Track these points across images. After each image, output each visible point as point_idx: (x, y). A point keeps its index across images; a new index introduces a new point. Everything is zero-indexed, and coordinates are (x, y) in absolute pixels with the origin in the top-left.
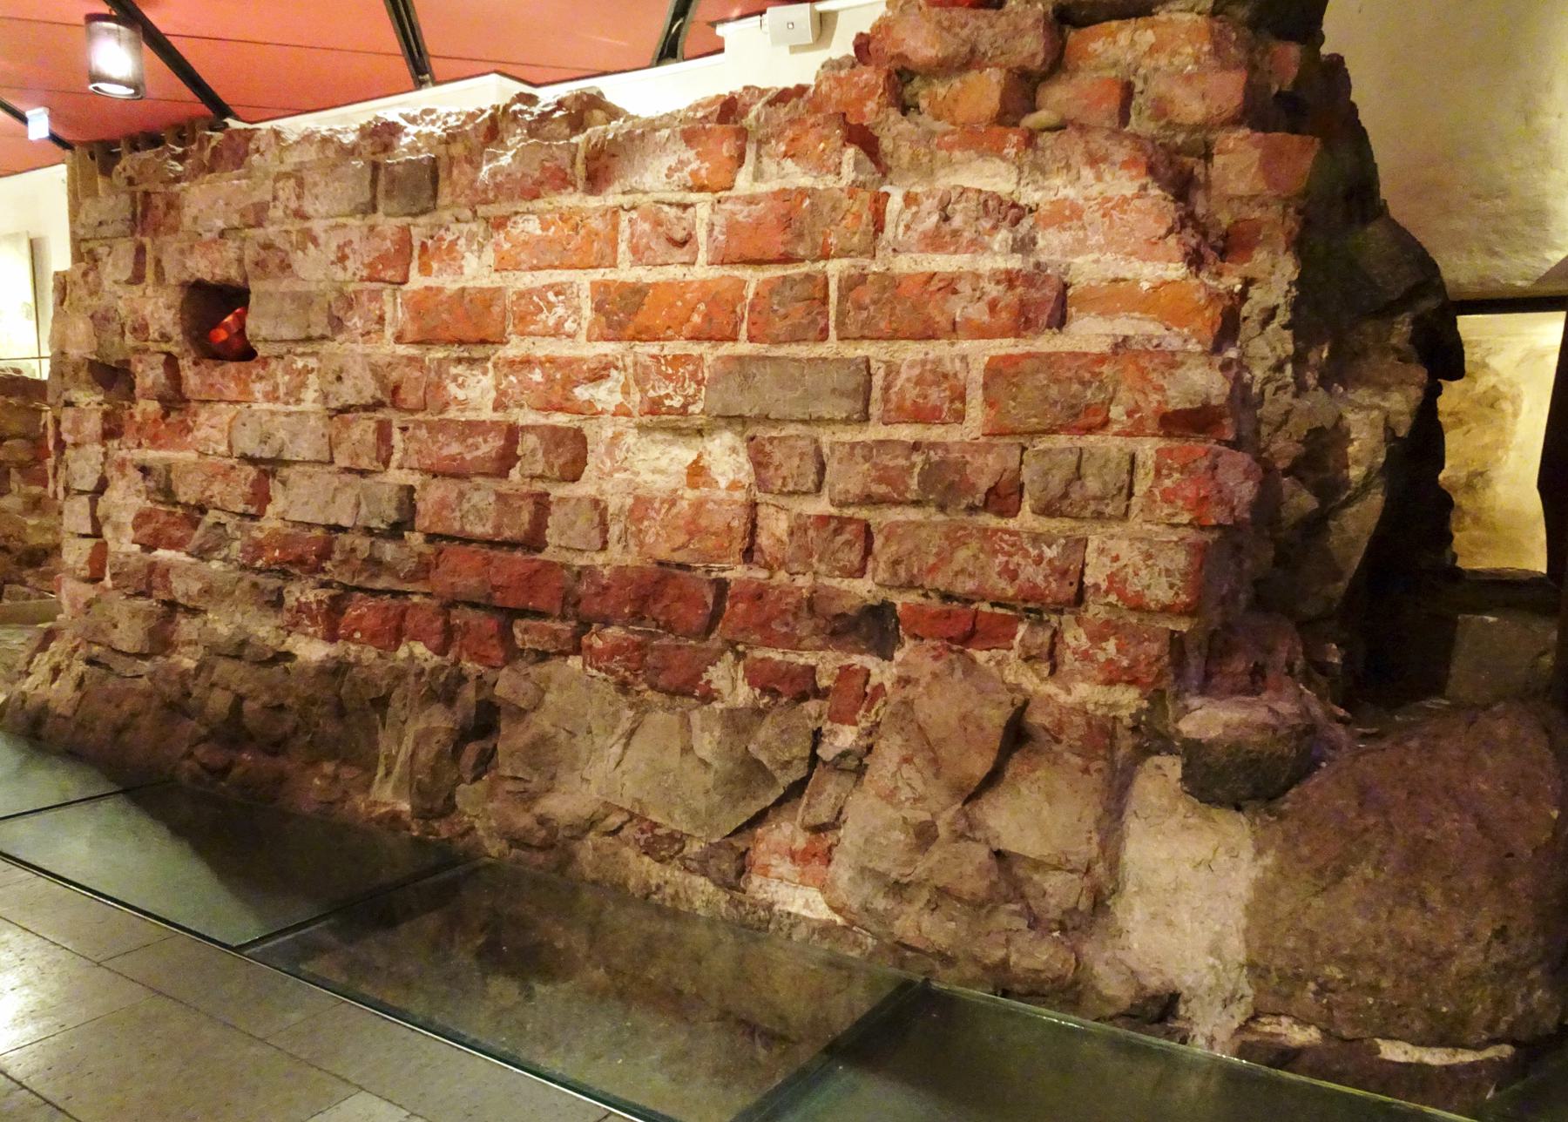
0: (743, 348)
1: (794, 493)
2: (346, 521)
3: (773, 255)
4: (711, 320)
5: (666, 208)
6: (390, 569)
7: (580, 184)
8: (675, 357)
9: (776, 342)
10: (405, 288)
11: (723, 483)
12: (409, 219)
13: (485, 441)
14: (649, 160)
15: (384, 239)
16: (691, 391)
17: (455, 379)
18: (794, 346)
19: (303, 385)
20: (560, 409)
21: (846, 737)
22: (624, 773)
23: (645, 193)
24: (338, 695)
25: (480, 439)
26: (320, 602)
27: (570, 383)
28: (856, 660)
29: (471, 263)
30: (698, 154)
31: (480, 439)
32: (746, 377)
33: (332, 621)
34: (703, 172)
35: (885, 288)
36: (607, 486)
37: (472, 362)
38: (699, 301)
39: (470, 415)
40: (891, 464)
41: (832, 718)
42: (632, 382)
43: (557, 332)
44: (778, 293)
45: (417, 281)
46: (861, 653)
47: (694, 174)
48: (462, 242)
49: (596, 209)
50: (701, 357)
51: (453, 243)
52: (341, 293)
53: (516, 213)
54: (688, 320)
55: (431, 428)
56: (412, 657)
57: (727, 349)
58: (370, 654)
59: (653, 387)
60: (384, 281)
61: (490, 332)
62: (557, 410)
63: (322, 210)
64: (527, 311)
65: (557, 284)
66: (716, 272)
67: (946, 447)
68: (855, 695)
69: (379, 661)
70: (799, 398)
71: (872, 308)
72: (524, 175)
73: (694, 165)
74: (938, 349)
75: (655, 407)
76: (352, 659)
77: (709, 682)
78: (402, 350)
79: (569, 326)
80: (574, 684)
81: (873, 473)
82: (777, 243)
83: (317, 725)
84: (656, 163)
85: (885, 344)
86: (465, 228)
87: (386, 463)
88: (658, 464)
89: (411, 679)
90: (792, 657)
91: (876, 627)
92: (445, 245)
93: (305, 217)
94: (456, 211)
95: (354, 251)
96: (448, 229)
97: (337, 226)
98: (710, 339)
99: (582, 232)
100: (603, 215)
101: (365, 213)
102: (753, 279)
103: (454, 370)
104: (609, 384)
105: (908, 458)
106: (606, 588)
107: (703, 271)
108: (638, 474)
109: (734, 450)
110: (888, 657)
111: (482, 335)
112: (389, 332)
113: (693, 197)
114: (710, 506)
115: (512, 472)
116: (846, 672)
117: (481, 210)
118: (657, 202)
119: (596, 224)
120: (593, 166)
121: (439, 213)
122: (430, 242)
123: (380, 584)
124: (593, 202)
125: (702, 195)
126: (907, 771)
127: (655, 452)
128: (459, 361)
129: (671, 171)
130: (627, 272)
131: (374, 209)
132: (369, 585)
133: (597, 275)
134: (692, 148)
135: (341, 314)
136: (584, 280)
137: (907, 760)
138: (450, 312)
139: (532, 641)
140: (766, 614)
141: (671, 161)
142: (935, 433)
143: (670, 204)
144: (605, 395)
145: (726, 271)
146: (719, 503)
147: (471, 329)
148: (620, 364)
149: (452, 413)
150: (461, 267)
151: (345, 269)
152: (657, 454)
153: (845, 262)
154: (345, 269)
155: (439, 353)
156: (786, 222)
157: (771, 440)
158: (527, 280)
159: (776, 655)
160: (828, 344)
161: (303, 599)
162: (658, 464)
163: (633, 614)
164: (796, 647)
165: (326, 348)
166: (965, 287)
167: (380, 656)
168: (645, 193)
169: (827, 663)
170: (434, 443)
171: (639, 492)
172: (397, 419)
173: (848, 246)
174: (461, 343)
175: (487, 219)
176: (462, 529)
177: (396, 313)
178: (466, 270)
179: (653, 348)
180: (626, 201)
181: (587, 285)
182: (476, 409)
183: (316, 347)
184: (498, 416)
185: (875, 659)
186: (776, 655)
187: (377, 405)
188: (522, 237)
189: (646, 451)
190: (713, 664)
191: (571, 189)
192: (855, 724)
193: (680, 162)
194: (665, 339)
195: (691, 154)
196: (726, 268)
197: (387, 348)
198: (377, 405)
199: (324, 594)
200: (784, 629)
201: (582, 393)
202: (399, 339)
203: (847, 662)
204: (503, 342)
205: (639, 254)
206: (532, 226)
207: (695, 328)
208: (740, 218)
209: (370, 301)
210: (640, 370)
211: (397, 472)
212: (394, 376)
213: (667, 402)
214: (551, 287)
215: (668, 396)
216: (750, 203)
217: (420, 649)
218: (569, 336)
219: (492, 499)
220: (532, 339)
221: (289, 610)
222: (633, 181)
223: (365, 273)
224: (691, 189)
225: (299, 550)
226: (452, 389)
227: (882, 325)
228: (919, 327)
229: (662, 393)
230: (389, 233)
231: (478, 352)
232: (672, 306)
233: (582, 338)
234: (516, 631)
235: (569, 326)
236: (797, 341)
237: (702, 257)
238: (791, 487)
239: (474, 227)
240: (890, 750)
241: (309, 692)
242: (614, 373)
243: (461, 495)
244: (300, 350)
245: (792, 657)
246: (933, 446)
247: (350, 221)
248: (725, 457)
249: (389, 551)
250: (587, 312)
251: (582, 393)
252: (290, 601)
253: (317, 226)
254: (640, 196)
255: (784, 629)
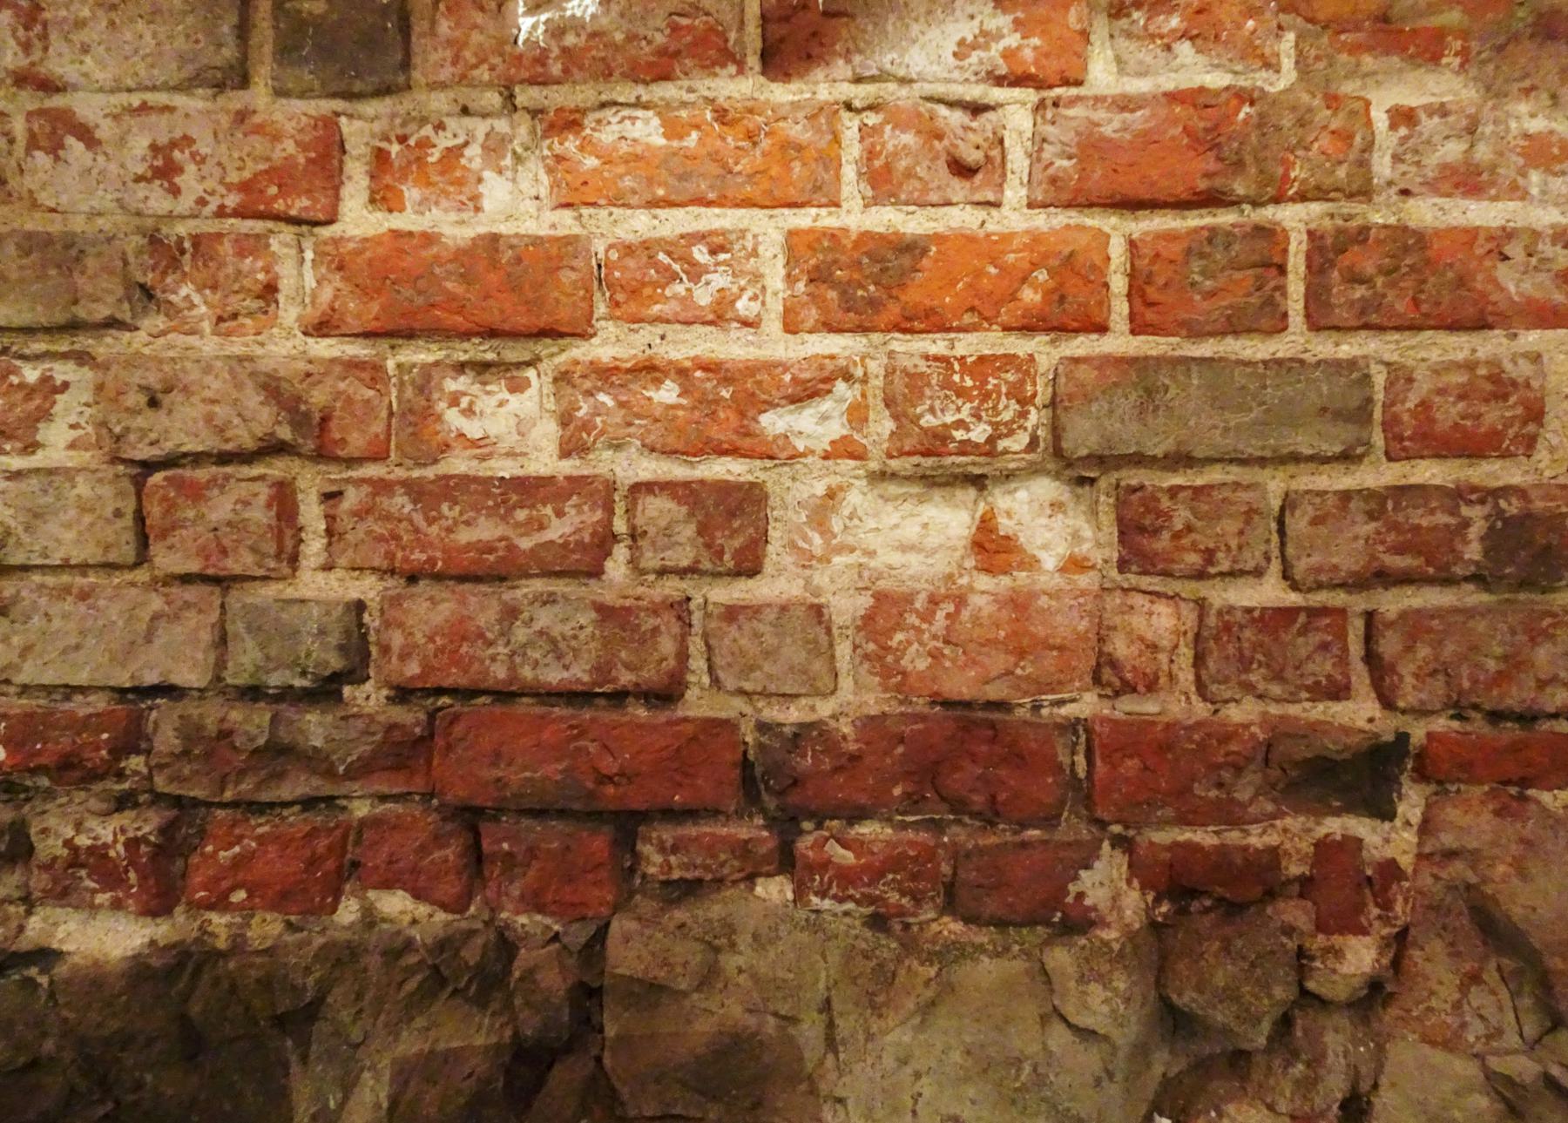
0: (1119, 342)
1: (1232, 574)
2: (189, 676)
3: (1181, 190)
4: (1062, 299)
5: (943, 111)
6: (316, 762)
7: (753, 61)
8: (982, 359)
9: (1195, 332)
10: (325, 232)
11: (1049, 562)
12: (338, 105)
13: (560, 514)
14: (915, 29)
15: (276, 138)
16: (1007, 416)
17: (454, 401)
18: (1230, 340)
19: (44, 415)
20: (734, 452)
21: (1361, 957)
22: (918, 1075)
23: (905, 81)
24: (184, 1019)
25: (548, 510)
26: (133, 844)
27: (751, 403)
28: (1333, 826)
29: (496, 192)
30: (1017, 22)
31: (548, 510)
32: (1149, 392)
33: (159, 878)
34: (1028, 54)
35: (1406, 249)
36: (821, 578)
37: (482, 368)
38: (1035, 266)
39: (505, 469)
40: (1424, 523)
41: (1321, 927)
42: (876, 403)
43: (720, 315)
44: (1202, 255)
45: (358, 219)
46: (1337, 813)
47: (1008, 54)
48: (474, 151)
49: (795, 106)
50: (1031, 358)
51: (454, 153)
52: (154, 240)
53: (603, 105)
54: (1014, 297)
55: (415, 490)
56: (370, 919)
57: (1081, 345)
58: (267, 928)
59: (932, 410)
60: (277, 218)
61: (564, 315)
62: (725, 453)
63: (102, 76)
64: (636, 283)
65: (712, 233)
66: (1041, 221)
67: (1521, 492)
68: (1346, 888)
69: (290, 938)
70: (1254, 423)
71: (1380, 281)
72: (631, 38)
73: (1013, 40)
74: (1490, 345)
75: (936, 443)
76: (222, 944)
77: (1080, 896)
78: (325, 348)
79: (743, 306)
80: (783, 930)
81: (1391, 538)
82: (1197, 171)
83: (139, 1086)
84: (934, 33)
85: (1397, 336)
86: (481, 127)
87: (294, 560)
88: (917, 537)
89: (373, 961)
90: (1233, 836)
91: (1367, 776)
92: (434, 156)
93: (49, 86)
94: (465, 95)
95: (200, 160)
96: (440, 127)
97: (145, 107)
98: (1048, 330)
99: (765, 143)
100: (811, 118)
101: (220, 87)
102: (1118, 232)
103: (451, 385)
104: (826, 405)
105: (1454, 512)
106: (855, 758)
107: (1015, 216)
108: (871, 554)
109: (1057, 506)
110: (1388, 814)
111: (543, 321)
112: (289, 313)
113: (998, 94)
114: (1043, 601)
115: (609, 565)
116: (1325, 848)
117: (525, 96)
118: (930, 99)
119: (797, 131)
120: (778, 30)
121: (420, 96)
122: (395, 149)
123: (286, 791)
124: (781, 93)
125: (1017, 93)
126: (1477, 997)
127: (891, 515)
128: (461, 368)
129: (963, 50)
130: (857, 215)
131: (244, 82)
132: (265, 797)
133: (803, 219)
134: (1005, 11)
135: (149, 278)
136: (768, 230)
137: (1475, 978)
138: (465, 278)
139: (685, 867)
140: (1168, 768)
141: (968, 30)
142: (1489, 472)
143: (951, 104)
144: (813, 425)
145: (1072, 217)
146: (1055, 595)
147: (513, 309)
148: (859, 372)
149: (459, 464)
150: (475, 198)
151: (175, 191)
152: (895, 518)
153: (1316, 208)
154: (175, 191)
155: (421, 354)
156: (1209, 141)
157: (1173, 492)
158: (639, 224)
159: (1204, 837)
160: (1287, 337)
161: (83, 841)
162: (917, 537)
163: (907, 795)
164: (1229, 814)
165: (106, 346)
166: (1515, 250)
167: (290, 926)
168: (905, 81)
169: (1293, 835)
170: (431, 521)
171: (882, 584)
172: (310, 482)
173: (1328, 182)
174: (492, 333)
175: (535, 113)
176: (514, 675)
177: (300, 275)
178: (486, 204)
179: (937, 345)
180: (861, 94)
181: (779, 238)
182: (511, 454)
183: (84, 342)
184: (569, 467)
185: (1367, 820)
186: (1204, 837)
187: (273, 448)
188: (624, 148)
189: (876, 515)
190: (1087, 867)
191: (732, 69)
192: (1363, 931)
193: (984, 33)
194: (960, 330)
195: (1003, 21)
196: (1073, 213)
197: (285, 345)
198: (273, 448)
199: (148, 824)
200: (1213, 793)
201: (773, 422)
202: (322, 327)
203: (1321, 831)
204: (582, 332)
205: (883, 182)
206: (647, 130)
207: (1027, 312)
208: (1107, 131)
209: (241, 254)
210: (899, 382)
211: (320, 577)
212: (318, 397)
213: (959, 435)
214: (700, 237)
215: (960, 424)
216: (1123, 109)
217: (395, 904)
218: (746, 323)
219: (586, 618)
220: (660, 329)
221: (47, 867)
222: (887, 59)
223: (232, 200)
224: (999, 81)
225: (65, 742)
226: (453, 419)
227: (1400, 307)
228: (1470, 311)
229: (949, 418)
230: (290, 127)
231: (514, 352)
232: (979, 273)
233: (773, 325)
234: (646, 849)
235: (743, 306)
236: (1236, 333)
237: (1014, 193)
238: (1225, 566)
239: (502, 125)
240: (1435, 966)
241: (114, 1025)
242: (840, 386)
243: (511, 613)
244: (39, 346)
245: (1233, 836)
246: (1506, 491)
247: (179, 100)
248: (1052, 528)
249: (315, 727)
250: (775, 277)
251: (773, 422)
252: (50, 847)
253: (87, 107)
254: (892, 86)
255: (1213, 793)
